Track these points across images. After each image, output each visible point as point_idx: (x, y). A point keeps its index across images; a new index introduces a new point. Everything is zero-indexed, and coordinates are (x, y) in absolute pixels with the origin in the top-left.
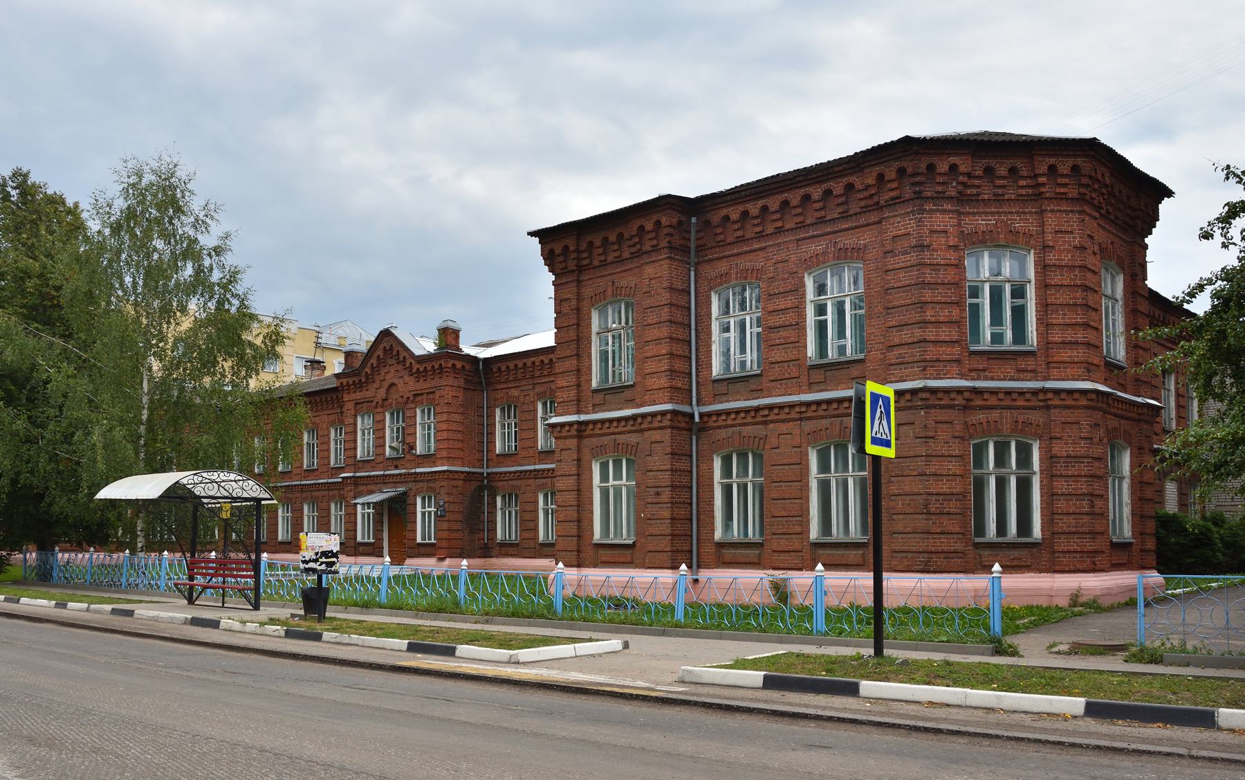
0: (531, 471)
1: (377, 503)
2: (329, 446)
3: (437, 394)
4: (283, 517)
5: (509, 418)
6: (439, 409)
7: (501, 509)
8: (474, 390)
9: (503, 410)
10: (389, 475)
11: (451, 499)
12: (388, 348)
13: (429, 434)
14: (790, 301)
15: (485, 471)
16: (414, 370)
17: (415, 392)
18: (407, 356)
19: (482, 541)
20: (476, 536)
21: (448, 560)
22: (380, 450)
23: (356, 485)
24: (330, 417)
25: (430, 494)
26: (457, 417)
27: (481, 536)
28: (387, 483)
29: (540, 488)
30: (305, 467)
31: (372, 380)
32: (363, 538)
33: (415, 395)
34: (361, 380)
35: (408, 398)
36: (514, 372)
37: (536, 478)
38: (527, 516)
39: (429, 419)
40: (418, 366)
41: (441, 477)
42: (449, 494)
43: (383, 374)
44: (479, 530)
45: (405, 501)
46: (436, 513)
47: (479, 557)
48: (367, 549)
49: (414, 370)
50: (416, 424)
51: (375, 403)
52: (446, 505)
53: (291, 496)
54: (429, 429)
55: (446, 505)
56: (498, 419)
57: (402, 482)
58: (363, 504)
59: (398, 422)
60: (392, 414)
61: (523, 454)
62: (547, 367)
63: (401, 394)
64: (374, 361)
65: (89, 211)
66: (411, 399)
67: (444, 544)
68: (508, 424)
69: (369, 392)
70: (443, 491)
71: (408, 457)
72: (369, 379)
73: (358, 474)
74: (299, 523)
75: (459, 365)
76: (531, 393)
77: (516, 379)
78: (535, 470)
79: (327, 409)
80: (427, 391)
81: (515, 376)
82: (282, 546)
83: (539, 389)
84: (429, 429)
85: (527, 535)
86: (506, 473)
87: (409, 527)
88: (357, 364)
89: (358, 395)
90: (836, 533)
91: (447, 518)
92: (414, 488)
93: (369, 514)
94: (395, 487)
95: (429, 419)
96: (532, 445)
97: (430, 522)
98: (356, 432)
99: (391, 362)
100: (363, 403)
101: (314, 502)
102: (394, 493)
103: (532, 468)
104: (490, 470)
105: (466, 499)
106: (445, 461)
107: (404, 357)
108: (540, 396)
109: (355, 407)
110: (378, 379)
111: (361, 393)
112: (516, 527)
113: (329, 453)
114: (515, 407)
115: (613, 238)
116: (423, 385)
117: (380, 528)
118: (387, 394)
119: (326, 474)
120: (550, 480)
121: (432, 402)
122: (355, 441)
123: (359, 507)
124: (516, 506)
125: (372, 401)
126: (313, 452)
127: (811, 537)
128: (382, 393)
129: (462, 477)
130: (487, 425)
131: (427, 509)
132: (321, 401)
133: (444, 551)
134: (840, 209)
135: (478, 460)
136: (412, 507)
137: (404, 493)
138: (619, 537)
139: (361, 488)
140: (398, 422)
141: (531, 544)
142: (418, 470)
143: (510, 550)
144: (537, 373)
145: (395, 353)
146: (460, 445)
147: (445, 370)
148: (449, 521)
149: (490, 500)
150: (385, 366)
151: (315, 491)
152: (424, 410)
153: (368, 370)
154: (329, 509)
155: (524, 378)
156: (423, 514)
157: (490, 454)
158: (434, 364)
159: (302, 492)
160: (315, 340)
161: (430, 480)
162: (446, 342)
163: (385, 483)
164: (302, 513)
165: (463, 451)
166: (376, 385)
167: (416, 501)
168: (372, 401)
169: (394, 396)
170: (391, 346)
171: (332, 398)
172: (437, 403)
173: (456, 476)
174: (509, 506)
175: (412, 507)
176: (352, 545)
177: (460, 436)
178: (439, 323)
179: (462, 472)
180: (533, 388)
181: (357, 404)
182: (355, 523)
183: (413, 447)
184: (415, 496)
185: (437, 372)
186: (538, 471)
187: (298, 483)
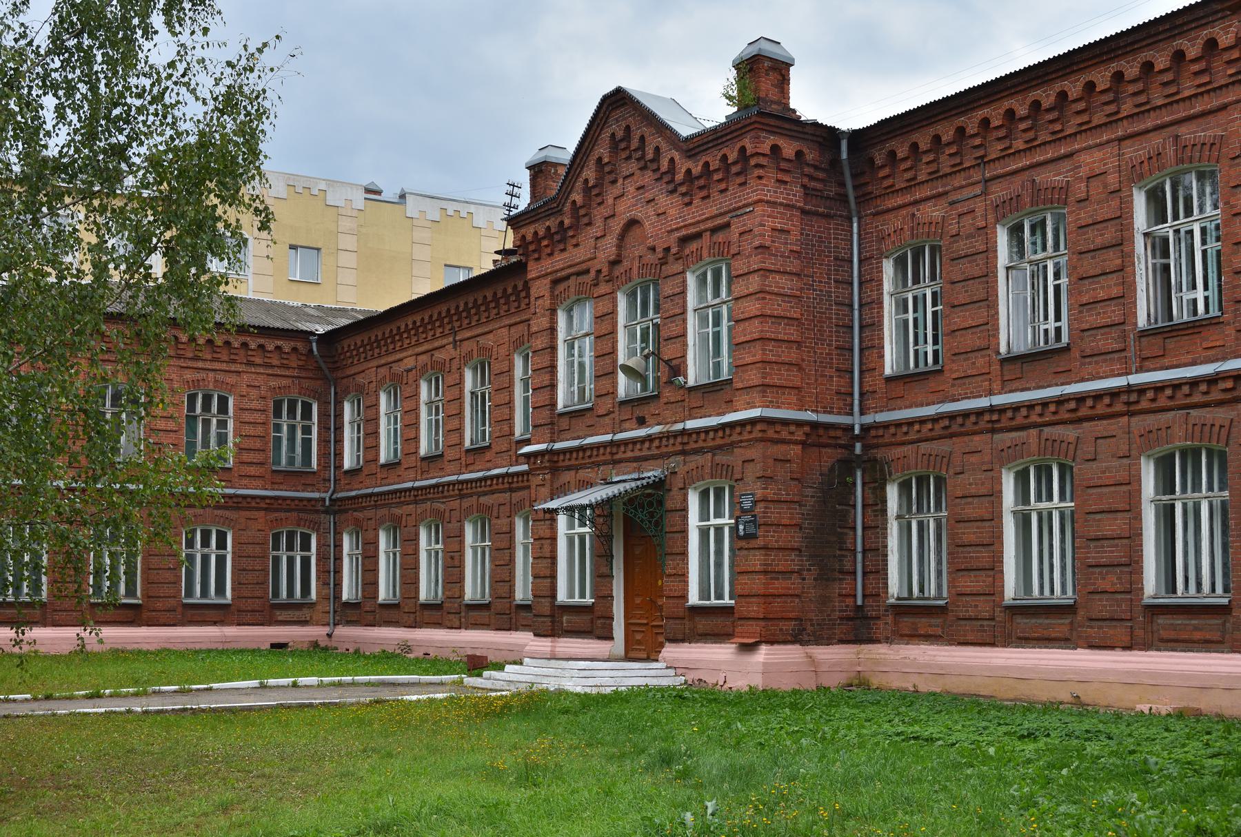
0: (980, 413)
1: (598, 504)
2: (511, 394)
3: (735, 230)
4: (429, 552)
5: (916, 280)
6: (741, 266)
7: (899, 517)
8: (827, 216)
9: (900, 263)
10: (625, 443)
11: (771, 493)
12: (620, 134)
13: (717, 336)
14: (1112, 260)
15: (857, 421)
16: (680, 177)
17: (684, 232)
18: (664, 146)
19: (849, 601)
20: (836, 588)
21: (764, 649)
22: (605, 384)
23: (555, 470)
24: (513, 330)
25: (719, 482)
26: (786, 284)
27: (845, 587)
28: (620, 461)
29: (1004, 457)
30: (467, 444)
31: (585, 220)
32: (571, 595)
33: (684, 240)
34: (562, 223)
35: (667, 250)
36: (931, 157)
37: (993, 431)
38: (969, 534)
39: (717, 293)
40: (689, 164)
41: (746, 436)
42: (766, 479)
43: (610, 201)
44: (841, 572)
45: (660, 503)
46: (734, 529)
47: (842, 642)
48: (581, 621)
49: (680, 177)
50: (684, 312)
51: (593, 274)
52: (759, 509)
53: (442, 507)
54: (717, 322)
55: (759, 509)
56: (887, 286)
57: (654, 457)
58: (570, 510)
59: (645, 312)
60: (632, 296)
61: (956, 369)
62: (1023, 126)
63: (650, 242)
64: (589, 173)
65: (736, 481)
66: (674, 250)
67: (755, 608)
68: (915, 298)
69: (581, 249)
70: (752, 472)
71: (668, 394)
72: (581, 218)
73: (558, 446)
74: (457, 563)
75: (789, 149)
76: (979, 206)
77: (935, 176)
78: (992, 409)
79: (508, 314)
80: (710, 224)
81: (933, 167)
82: (426, 613)
83: (999, 192)
84: (717, 322)
85: (969, 583)
86: (910, 423)
87: (670, 565)
88: (554, 187)
89: (558, 261)
90: (1184, 594)
91: (760, 542)
92: (681, 470)
93: (582, 538)
94: (639, 470)
95: (717, 293)
96: (984, 344)
97: (719, 552)
98: (553, 349)
99: (633, 166)
100: (567, 278)
101: (484, 516)
102: (633, 484)
103: (983, 402)
104: (869, 419)
105: (809, 492)
106: (756, 395)
107: (657, 149)
108: (1001, 210)
109: (552, 289)
110: (599, 213)
111: (566, 255)
112: (939, 562)
113: (512, 409)
114: (933, 250)
115: (1161, 62)
116: (703, 211)
117: (604, 570)
118: (619, 247)
119: (505, 456)
120: (1034, 432)
121: (724, 252)
122: (553, 368)
123: (562, 520)
124: (938, 507)
125: (587, 271)
126: (484, 412)
127: (1006, 597)
128: (609, 247)
129: (799, 435)
130: (861, 306)
131: (714, 521)
132: (495, 299)
133: (756, 627)
134: (1079, 120)
135: (838, 393)
136: (676, 517)
137: (659, 484)
138: (1045, 514)
139: (568, 476)
140: (645, 312)
141: (983, 607)
142: (691, 424)
143: (923, 624)
144: (995, 150)
145: (635, 143)
146: (792, 355)
147: (753, 162)
148: (765, 548)
149: (868, 491)
150: (614, 182)
151: (485, 494)
152: (705, 274)
153: (577, 197)
154: (511, 532)
155: (958, 169)
156: (704, 533)
157: (868, 379)
158: (725, 151)
159: (462, 497)
160: (507, 199)
161: (720, 447)
162: (756, 90)
163: (616, 462)
164: (462, 543)
165: (800, 368)
166: (595, 231)
167: (685, 500)
168: (587, 271)
169: (635, 250)
170: (628, 128)
171: (515, 287)
172: (734, 250)
173: (784, 434)
174: (920, 510)
175: (676, 517)
176: (546, 610)
177: (793, 333)
178: (738, 48)
179: (799, 424)
180: (985, 193)
181: (555, 282)
182: (553, 559)
183: (677, 369)
184: (684, 489)
185: (735, 169)
186: (1001, 410)
187: (454, 478)
